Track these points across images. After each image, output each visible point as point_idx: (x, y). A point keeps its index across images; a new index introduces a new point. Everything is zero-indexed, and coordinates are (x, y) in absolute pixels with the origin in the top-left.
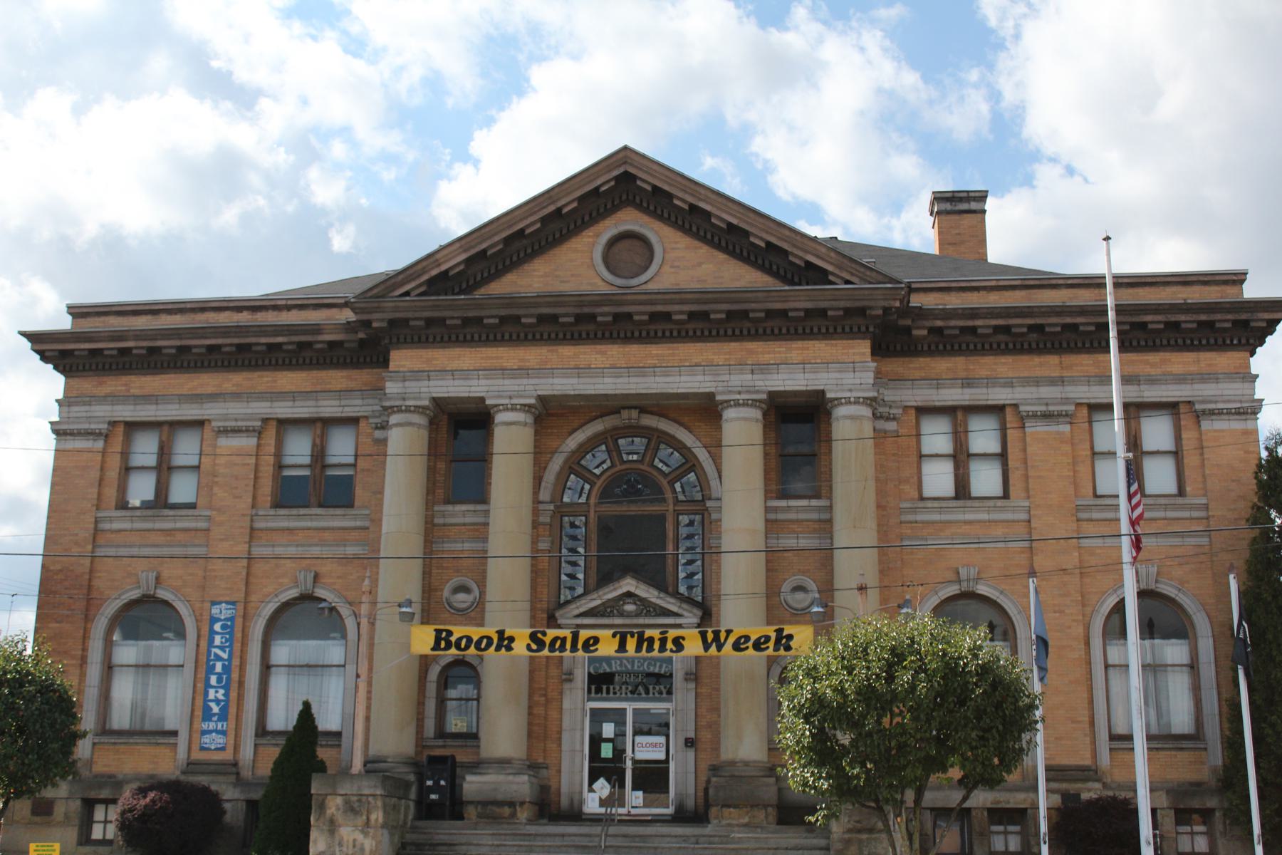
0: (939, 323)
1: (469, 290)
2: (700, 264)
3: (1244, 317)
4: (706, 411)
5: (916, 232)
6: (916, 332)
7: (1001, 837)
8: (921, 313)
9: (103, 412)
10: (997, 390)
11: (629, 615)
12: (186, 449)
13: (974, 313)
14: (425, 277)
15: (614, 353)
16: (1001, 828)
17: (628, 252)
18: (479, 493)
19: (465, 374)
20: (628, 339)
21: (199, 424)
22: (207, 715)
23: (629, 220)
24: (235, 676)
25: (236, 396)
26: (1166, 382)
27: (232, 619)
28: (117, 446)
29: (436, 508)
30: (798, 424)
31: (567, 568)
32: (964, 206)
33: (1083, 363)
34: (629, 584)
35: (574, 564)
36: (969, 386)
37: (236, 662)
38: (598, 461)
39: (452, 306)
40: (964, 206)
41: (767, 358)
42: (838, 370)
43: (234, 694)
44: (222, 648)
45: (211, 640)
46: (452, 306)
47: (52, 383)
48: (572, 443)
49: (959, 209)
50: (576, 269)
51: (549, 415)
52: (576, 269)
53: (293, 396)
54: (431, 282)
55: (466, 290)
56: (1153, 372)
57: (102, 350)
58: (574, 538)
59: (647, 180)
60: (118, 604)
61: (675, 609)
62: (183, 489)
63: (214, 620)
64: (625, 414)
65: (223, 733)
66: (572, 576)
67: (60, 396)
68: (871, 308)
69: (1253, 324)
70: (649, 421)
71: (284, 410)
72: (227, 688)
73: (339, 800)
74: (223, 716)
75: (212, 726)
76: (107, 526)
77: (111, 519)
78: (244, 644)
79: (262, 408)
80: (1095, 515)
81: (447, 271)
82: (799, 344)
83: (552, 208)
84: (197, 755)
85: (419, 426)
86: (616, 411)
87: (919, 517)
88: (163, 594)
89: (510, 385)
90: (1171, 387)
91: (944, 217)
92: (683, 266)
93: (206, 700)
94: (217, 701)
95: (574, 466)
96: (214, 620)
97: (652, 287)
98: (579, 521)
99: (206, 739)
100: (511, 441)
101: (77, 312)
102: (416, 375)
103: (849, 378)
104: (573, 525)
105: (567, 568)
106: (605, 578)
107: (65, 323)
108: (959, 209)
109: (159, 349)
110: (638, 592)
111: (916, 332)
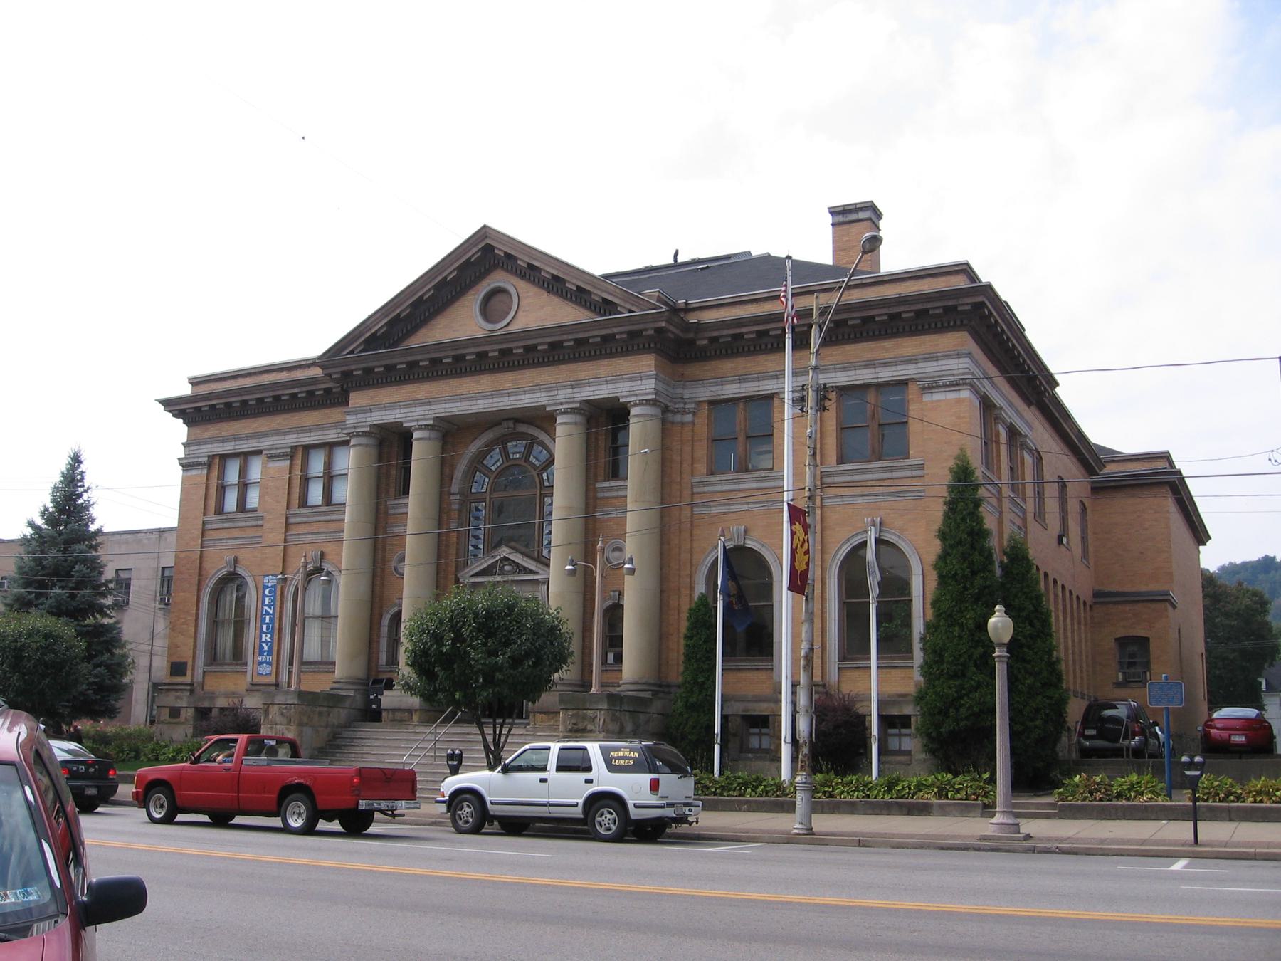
0: (715, 334)
1: (395, 344)
2: (542, 307)
3: (951, 303)
4: (543, 419)
5: (815, 245)
6: (699, 343)
7: (896, 739)
8: (699, 327)
9: (207, 449)
10: (766, 382)
11: (509, 573)
12: (256, 470)
13: (739, 323)
14: (362, 339)
15: (484, 383)
16: (756, 730)
17: (492, 305)
18: (616, 470)
19: (392, 406)
20: (493, 370)
21: (259, 452)
22: (261, 652)
23: (499, 279)
24: (277, 625)
25: (277, 433)
26: (896, 364)
27: (274, 586)
28: (298, 462)
29: (599, 485)
30: (607, 421)
31: (472, 541)
32: (853, 217)
33: (763, 362)
34: (505, 551)
35: (477, 538)
36: (745, 381)
37: (277, 615)
38: (494, 461)
39: (380, 357)
40: (853, 217)
41: (584, 375)
42: (632, 381)
43: (276, 637)
44: (269, 606)
45: (264, 601)
46: (380, 357)
47: (179, 429)
48: (473, 449)
49: (858, 220)
50: (463, 323)
51: (451, 432)
52: (463, 323)
53: (310, 429)
54: (367, 341)
55: (388, 345)
56: (887, 355)
57: (900, 313)
58: (477, 518)
59: (501, 248)
60: (215, 580)
61: (533, 568)
62: (253, 499)
63: (265, 587)
64: (505, 424)
65: (270, 663)
66: (476, 547)
67: (185, 440)
68: (646, 330)
69: (960, 308)
70: (523, 428)
71: (305, 439)
72: (272, 634)
73: (276, 707)
74: (270, 653)
75: (264, 659)
76: (209, 526)
77: (703, 484)
78: (282, 603)
79: (293, 439)
80: (837, 479)
81: (375, 333)
82: (605, 362)
83: (440, 278)
84: (257, 680)
85: (367, 446)
86: (499, 423)
87: (707, 489)
88: (750, 544)
89: (419, 412)
90: (900, 367)
91: (838, 228)
92: (536, 312)
93: (261, 642)
94: (266, 642)
95: (477, 464)
96: (265, 587)
97: (511, 328)
98: (481, 505)
99: (260, 668)
100: (422, 453)
101: (195, 382)
102: (364, 410)
103: (638, 386)
104: (477, 509)
105: (472, 541)
106: (494, 545)
107: (186, 390)
108: (858, 220)
109: (742, 335)
110: (510, 557)
111: (699, 343)
